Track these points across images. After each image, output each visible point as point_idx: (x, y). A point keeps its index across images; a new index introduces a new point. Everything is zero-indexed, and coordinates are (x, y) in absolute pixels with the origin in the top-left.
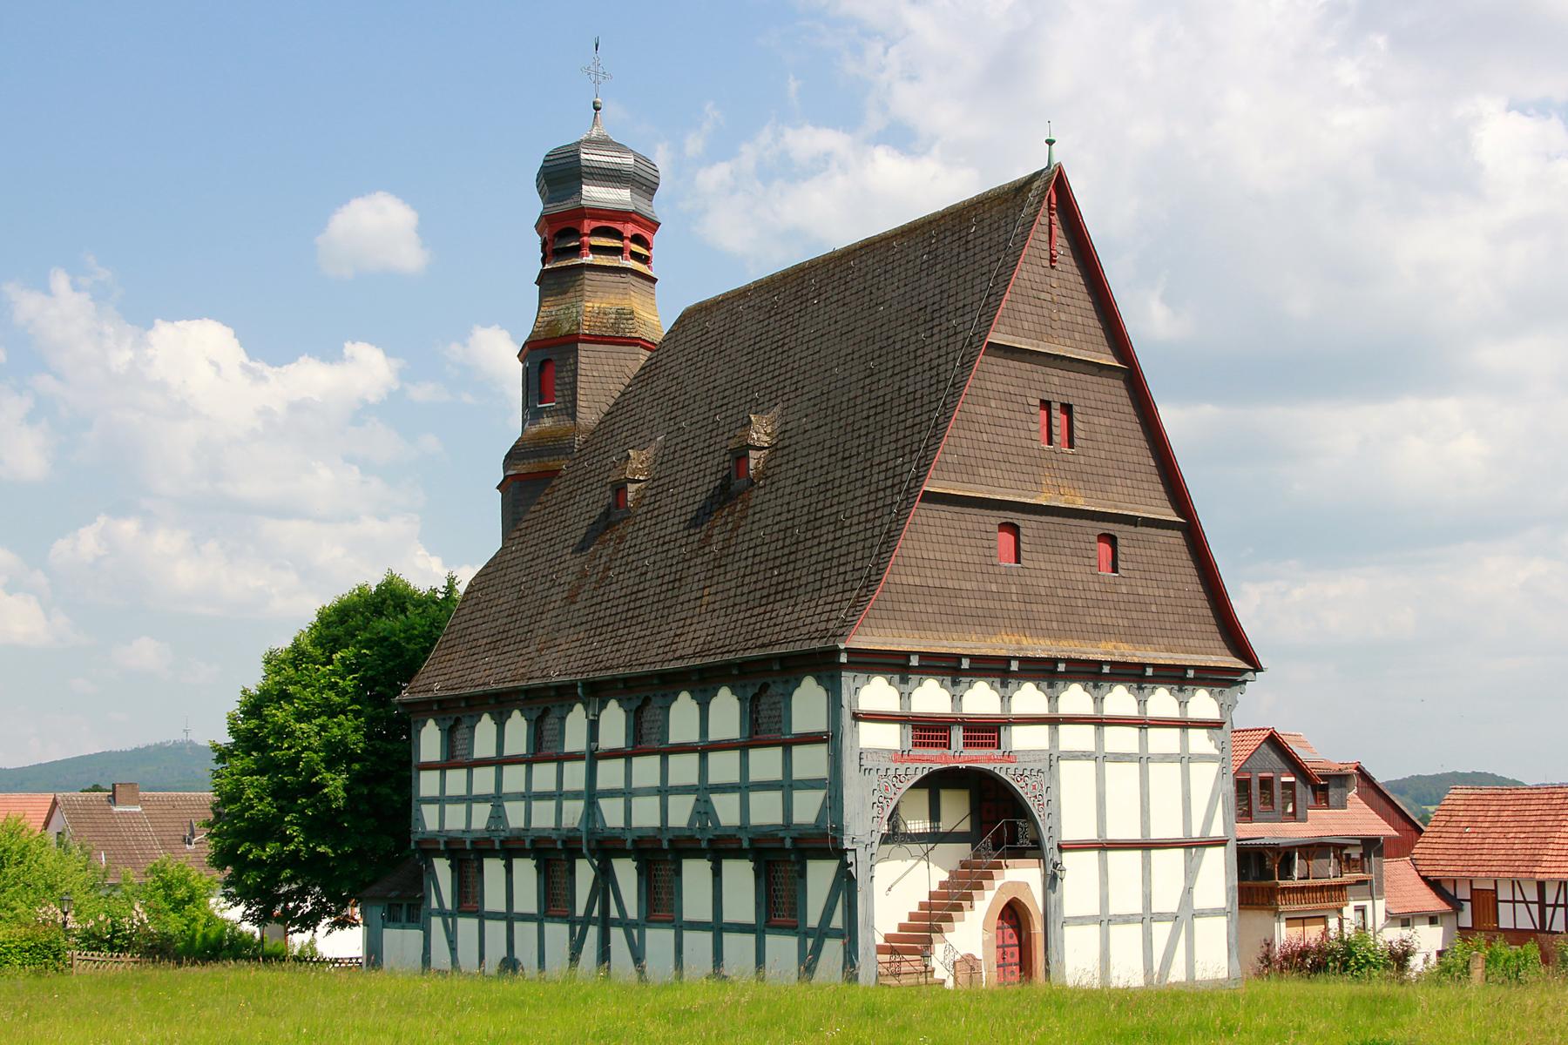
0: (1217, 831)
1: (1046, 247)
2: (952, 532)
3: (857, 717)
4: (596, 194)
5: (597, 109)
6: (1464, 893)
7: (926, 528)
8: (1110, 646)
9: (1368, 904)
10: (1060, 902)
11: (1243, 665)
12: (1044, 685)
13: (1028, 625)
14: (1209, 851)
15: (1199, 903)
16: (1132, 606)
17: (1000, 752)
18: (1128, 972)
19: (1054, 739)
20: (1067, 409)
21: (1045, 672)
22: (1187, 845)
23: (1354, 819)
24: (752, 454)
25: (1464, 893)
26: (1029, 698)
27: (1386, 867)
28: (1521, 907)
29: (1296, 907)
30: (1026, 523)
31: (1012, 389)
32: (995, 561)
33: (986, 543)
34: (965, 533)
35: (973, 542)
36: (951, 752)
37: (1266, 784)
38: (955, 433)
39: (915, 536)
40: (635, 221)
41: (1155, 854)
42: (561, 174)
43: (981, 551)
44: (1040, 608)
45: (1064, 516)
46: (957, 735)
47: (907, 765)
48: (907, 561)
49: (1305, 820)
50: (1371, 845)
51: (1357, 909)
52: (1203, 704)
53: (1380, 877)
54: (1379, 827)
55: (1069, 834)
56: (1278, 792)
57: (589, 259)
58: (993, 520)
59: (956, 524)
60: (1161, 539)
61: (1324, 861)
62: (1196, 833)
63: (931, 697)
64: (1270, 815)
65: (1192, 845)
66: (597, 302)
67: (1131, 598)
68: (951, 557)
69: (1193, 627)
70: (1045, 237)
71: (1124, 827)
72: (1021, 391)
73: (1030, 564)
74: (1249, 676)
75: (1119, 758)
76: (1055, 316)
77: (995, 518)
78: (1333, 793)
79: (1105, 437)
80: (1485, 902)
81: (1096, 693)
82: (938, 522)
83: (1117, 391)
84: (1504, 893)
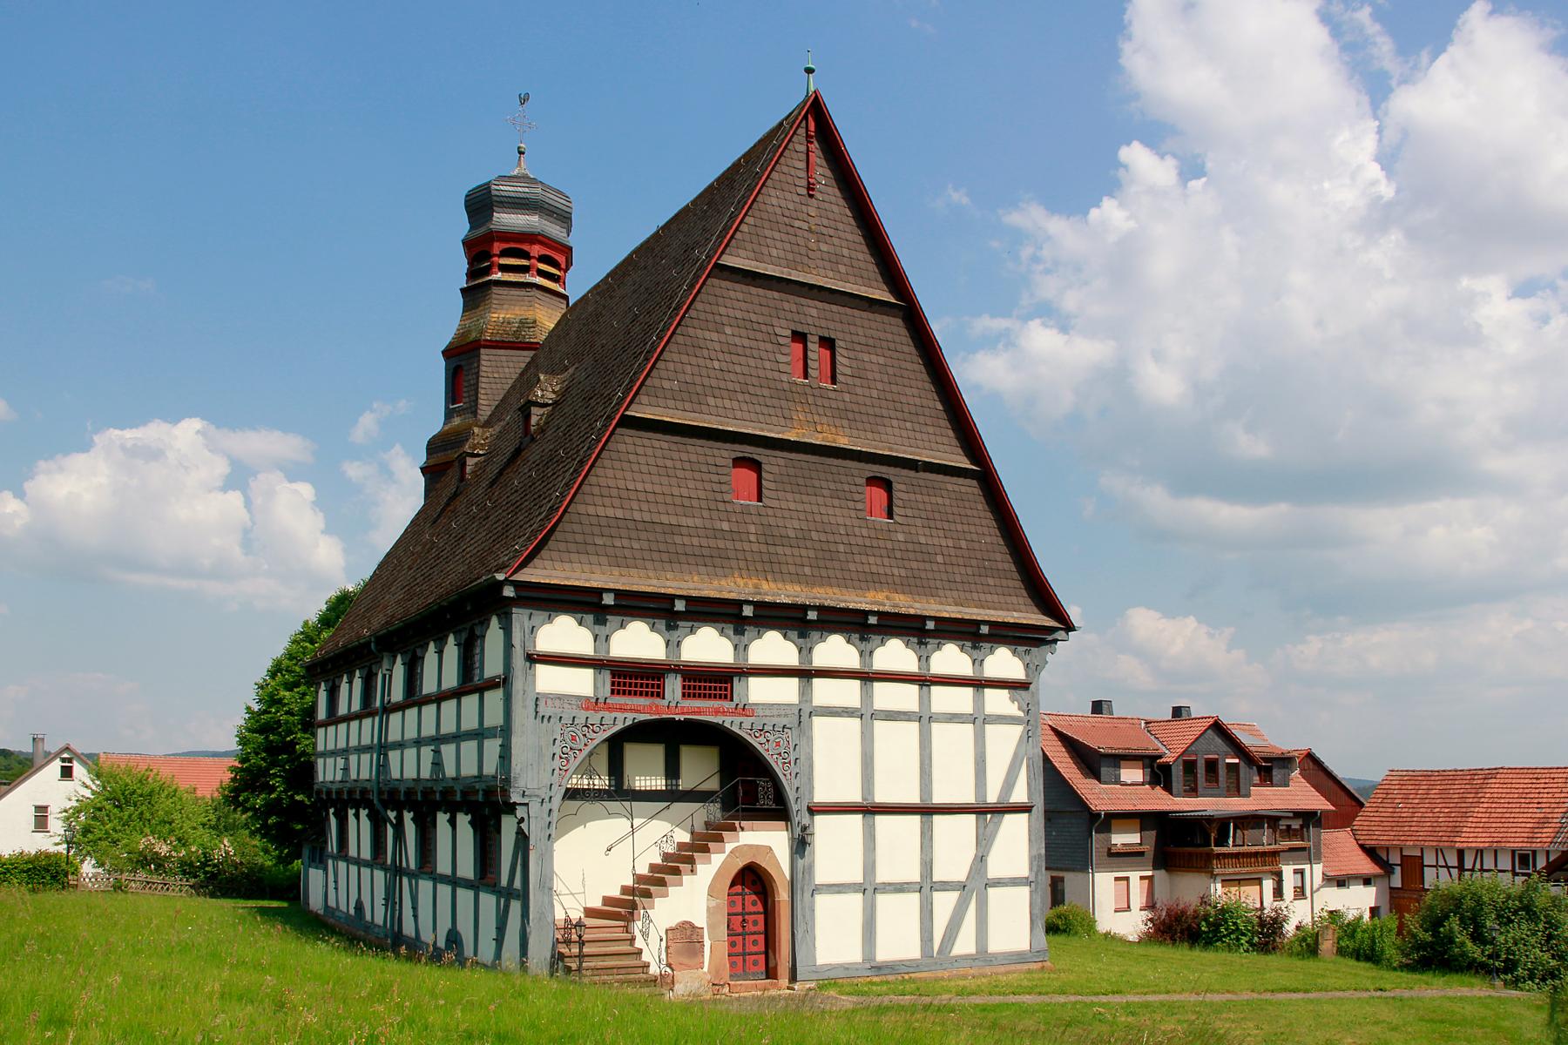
0: (1020, 795)
1: (803, 174)
2: (669, 463)
3: (534, 659)
4: (507, 220)
5: (521, 153)
6: (1395, 859)
7: (632, 457)
8: (881, 596)
9: (1307, 867)
10: (810, 869)
11: (1049, 622)
12: (794, 634)
13: (771, 567)
14: (1008, 817)
15: (995, 869)
16: (911, 555)
17: (733, 705)
18: (899, 939)
19: (805, 693)
20: (828, 343)
21: (795, 620)
22: (980, 810)
23: (1299, 794)
24: (534, 410)
25: (1395, 859)
26: (772, 647)
27: (1323, 836)
28: (1443, 871)
29: (1231, 870)
30: (773, 463)
31: (754, 317)
32: (727, 497)
33: (715, 478)
34: (687, 466)
35: (697, 476)
36: (665, 703)
37: (1212, 766)
38: (676, 357)
39: (617, 464)
40: (541, 243)
41: (938, 819)
42: (480, 204)
43: (708, 486)
44: (788, 551)
45: (821, 455)
46: (674, 686)
47: (601, 714)
48: (605, 492)
49: (1248, 795)
50: (1309, 818)
51: (1296, 872)
52: (1003, 662)
53: (1318, 845)
54: (1315, 801)
55: (821, 796)
56: (1222, 772)
57: (498, 276)
58: (725, 454)
59: (675, 455)
60: (950, 487)
61: (1256, 832)
62: (992, 798)
63: (638, 641)
64: (1216, 791)
65: (987, 812)
66: (503, 313)
67: (910, 547)
68: (666, 490)
69: (991, 581)
70: (803, 165)
71: (897, 786)
72: (768, 320)
73: (775, 504)
74: (1060, 635)
75: (892, 716)
76: (812, 245)
77: (725, 453)
78: (1277, 774)
79: (878, 376)
80: (1412, 867)
81: (863, 646)
82: (650, 451)
83: (895, 329)
84: (1429, 859)
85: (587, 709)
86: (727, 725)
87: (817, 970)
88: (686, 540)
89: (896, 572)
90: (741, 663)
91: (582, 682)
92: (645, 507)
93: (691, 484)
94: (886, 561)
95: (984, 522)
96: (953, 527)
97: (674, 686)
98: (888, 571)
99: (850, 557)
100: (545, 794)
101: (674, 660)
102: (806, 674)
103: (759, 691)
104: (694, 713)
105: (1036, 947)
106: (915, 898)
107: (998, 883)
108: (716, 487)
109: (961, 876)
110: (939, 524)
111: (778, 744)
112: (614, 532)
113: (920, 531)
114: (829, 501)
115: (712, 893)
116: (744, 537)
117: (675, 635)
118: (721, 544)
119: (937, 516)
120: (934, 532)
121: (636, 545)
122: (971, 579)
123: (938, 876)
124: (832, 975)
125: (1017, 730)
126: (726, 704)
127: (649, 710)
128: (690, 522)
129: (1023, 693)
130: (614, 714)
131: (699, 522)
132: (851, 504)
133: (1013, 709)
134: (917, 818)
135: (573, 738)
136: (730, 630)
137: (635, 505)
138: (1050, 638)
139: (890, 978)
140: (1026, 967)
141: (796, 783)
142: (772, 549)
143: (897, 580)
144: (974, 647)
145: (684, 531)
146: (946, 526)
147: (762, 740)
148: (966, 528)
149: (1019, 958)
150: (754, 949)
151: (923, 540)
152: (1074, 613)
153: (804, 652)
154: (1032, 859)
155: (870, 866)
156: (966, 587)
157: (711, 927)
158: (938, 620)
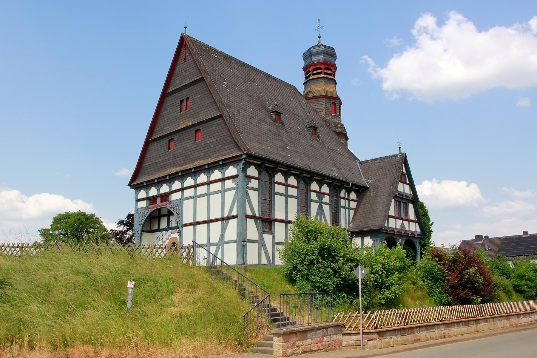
14: (231, 221)
65: (224, 220)
69: (226, 147)
109: (217, 241)
125: (234, 191)
126: (167, 202)
129: (236, 179)
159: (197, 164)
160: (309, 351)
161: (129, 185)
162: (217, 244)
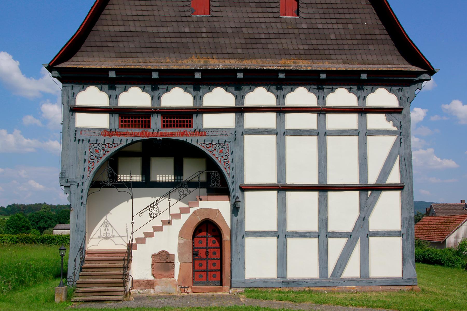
13: (216, 50)
14: (384, 194)
17: (192, 130)
22: (363, 188)
26: (219, 96)
41: (331, 194)
43: (176, 9)
44: (227, 41)
47: (113, 137)
52: (382, 97)
55: (249, 180)
62: (372, 180)
63: (135, 97)
65: (368, 191)
67: (311, 31)
69: (371, 47)
85: (105, 135)
86: (189, 141)
87: (245, 281)
88: (163, 40)
89: (301, 47)
90: (198, 106)
91: (102, 121)
92: (137, 24)
93: (166, 9)
94: (294, 41)
95: (366, 11)
96: (342, 16)
97: (156, 122)
98: (295, 47)
99: (268, 41)
100: (79, 181)
101: (156, 106)
102: (240, 110)
103: (209, 121)
104: (169, 135)
105: (408, 276)
106: (314, 242)
107: (377, 234)
108: (181, 9)
109: (349, 228)
110: (332, 16)
111: (221, 151)
112: (118, 39)
113: (319, 21)
114: (254, 10)
115: (181, 235)
116: (198, 35)
117: (156, 93)
118: (184, 40)
119: (331, 11)
120: (329, 21)
121: (132, 45)
122: (356, 47)
123: (331, 228)
124: (255, 285)
125: (392, 139)
126: (188, 130)
127: (142, 134)
128: (165, 30)
129: (397, 116)
130: (121, 138)
131: (170, 29)
132: (269, 10)
133: (389, 126)
134: (315, 194)
135: (97, 151)
136: (191, 89)
137: (131, 23)
138: (417, 79)
139: (295, 289)
140: (398, 288)
141: (232, 173)
142: (216, 40)
143: (302, 52)
144: (359, 89)
145: (161, 35)
146: (338, 16)
147: (211, 149)
148: (353, 16)
149: (393, 282)
150: (214, 268)
151: (320, 26)
152: (434, 65)
153: (239, 98)
154: (403, 220)
155: (282, 221)
156: (352, 52)
157: (180, 255)
158: (328, 73)
159: (290, 64)
160: (81, 301)
161: (50, 68)
162: (349, 235)
